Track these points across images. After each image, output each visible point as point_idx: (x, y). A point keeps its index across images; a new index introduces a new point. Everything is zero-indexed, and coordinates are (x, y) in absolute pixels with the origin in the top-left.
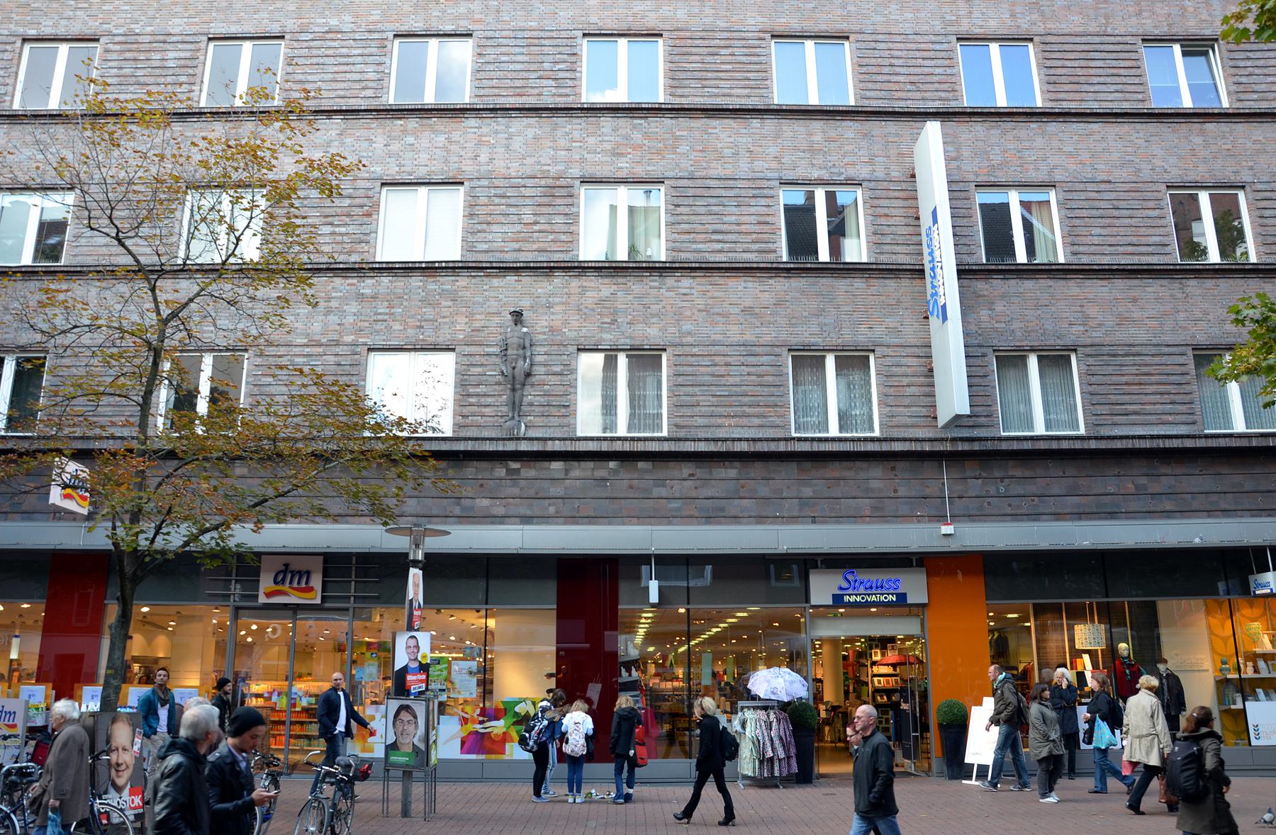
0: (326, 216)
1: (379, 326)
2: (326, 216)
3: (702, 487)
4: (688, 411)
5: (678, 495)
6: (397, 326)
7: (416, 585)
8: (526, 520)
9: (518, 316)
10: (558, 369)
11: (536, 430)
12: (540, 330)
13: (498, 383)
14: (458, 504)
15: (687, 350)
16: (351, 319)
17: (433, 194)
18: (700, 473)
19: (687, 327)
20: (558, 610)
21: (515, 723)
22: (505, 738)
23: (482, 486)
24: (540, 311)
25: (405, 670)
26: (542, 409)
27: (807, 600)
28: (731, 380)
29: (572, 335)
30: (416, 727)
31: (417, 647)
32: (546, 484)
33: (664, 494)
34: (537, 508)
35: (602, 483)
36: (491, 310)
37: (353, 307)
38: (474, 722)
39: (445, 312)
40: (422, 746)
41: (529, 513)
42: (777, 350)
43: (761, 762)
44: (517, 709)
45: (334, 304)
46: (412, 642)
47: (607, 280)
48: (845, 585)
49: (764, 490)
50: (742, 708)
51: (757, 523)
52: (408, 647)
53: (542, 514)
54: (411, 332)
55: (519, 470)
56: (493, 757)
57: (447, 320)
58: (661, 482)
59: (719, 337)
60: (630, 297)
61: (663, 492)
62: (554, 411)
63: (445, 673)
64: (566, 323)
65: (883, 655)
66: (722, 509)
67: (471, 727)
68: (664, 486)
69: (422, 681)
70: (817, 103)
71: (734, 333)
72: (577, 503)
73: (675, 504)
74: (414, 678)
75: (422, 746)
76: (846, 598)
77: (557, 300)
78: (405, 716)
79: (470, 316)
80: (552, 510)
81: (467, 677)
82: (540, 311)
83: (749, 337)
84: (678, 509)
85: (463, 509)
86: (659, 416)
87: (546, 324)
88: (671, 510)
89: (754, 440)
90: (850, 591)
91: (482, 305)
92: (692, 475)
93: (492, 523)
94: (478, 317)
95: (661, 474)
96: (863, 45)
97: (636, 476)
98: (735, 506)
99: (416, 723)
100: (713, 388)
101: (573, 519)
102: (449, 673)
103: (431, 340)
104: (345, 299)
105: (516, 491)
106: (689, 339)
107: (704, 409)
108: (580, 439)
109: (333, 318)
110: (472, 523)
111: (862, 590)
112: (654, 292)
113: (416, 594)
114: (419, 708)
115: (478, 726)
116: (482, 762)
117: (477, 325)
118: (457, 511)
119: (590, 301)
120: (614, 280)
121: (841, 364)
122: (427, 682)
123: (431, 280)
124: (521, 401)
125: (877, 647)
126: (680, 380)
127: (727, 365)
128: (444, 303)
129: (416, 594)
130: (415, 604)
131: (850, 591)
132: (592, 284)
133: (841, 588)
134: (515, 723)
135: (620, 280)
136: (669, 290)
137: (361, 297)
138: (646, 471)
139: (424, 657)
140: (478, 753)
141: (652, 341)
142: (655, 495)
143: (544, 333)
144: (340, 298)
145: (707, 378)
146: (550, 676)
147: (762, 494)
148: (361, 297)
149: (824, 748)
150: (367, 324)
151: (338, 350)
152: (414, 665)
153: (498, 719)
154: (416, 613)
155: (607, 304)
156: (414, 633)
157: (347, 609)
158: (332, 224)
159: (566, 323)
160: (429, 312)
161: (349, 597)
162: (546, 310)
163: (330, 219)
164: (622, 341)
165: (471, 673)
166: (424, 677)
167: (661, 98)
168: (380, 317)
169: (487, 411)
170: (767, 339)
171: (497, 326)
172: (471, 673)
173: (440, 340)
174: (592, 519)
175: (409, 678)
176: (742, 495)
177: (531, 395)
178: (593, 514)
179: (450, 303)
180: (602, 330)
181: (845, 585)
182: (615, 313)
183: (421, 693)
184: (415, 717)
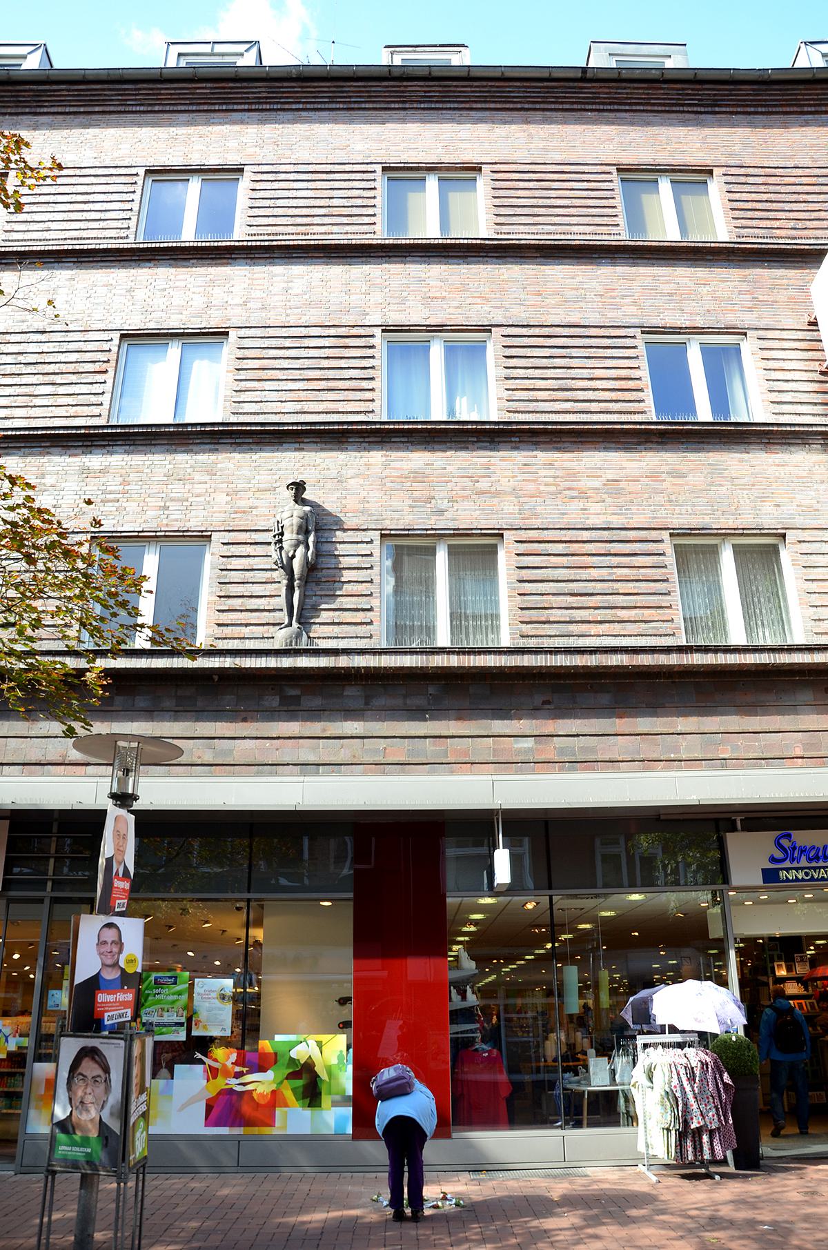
6: (132, 506)
7: (120, 836)
17: (190, 351)
20: (357, 900)
21: (291, 1076)
22: (275, 1099)
25: (94, 984)
27: (726, 880)
30: (108, 1089)
31: (119, 943)
36: (262, 486)
38: (227, 1074)
40: (115, 1126)
43: (682, 1136)
44: (293, 1054)
46: (110, 935)
48: (779, 854)
50: (646, 1046)
52: (101, 943)
55: (298, 698)
56: (255, 1130)
57: (202, 499)
63: (185, 997)
65: (789, 969)
67: (221, 1083)
69: (124, 1004)
70: (309, 1133)
74: (111, 998)
75: (115, 1126)
76: (783, 874)
78: (89, 1068)
81: (217, 1003)
88: (519, 751)
90: (787, 864)
96: (730, 179)
99: (107, 1082)
102: (191, 997)
111: (804, 862)
113: (120, 850)
114: (114, 1052)
115: (234, 1081)
116: (239, 1141)
117: (243, 504)
121: (740, 553)
122: (138, 1006)
125: (780, 959)
129: (120, 850)
130: (118, 868)
131: (787, 864)
133: (773, 859)
134: (291, 1076)
139: (131, 961)
140: (232, 1125)
146: (343, 1001)
149: (203, 1063)
152: (111, 975)
153: (262, 1069)
154: (118, 884)
156: (117, 920)
157: (41, 901)
161: (45, 882)
165: (223, 997)
166: (129, 997)
167: (445, 419)
172: (223, 997)
175: (101, 997)
178: (408, 760)
181: (779, 854)
183: (121, 1026)
184: (106, 1070)
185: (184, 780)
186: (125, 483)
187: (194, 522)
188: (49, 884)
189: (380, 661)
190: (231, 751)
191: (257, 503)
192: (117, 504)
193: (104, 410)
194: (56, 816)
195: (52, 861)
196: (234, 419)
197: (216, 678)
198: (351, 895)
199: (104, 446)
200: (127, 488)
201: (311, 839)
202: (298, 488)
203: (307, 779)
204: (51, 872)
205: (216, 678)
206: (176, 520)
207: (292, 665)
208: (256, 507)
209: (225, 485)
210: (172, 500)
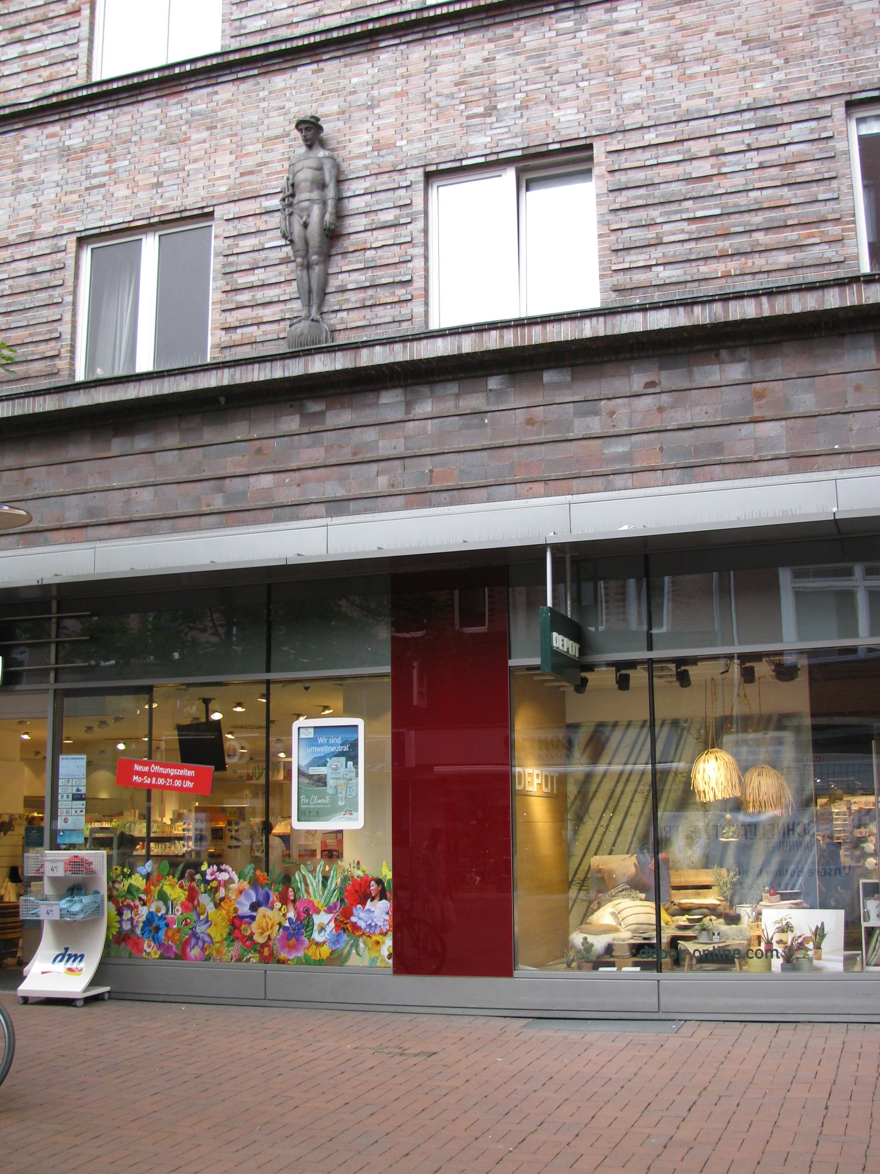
0: (13, 29)
1: (95, 197)
2: (13, 29)
3: (673, 406)
4: (639, 259)
5: (624, 428)
6: (121, 191)
8: (337, 506)
9: (311, 130)
10: (388, 217)
11: (362, 325)
12: (358, 151)
13: (285, 261)
14: (220, 490)
15: (635, 139)
16: (50, 194)
18: (668, 378)
19: (632, 94)
23: (259, 451)
24: (357, 115)
26: (361, 295)
28: (727, 184)
29: (417, 147)
32: (370, 435)
33: (597, 430)
34: (358, 480)
35: (475, 420)
36: (272, 133)
37: (54, 173)
39: (197, 151)
41: (341, 493)
42: (824, 108)
45: (27, 173)
47: (474, 37)
49: (805, 400)
51: (792, 471)
53: (364, 491)
54: (143, 196)
58: (588, 407)
59: (700, 103)
60: (521, 59)
61: (595, 425)
62: (384, 295)
64: (402, 127)
66: (718, 447)
68: (596, 413)
71: (729, 92)
72: (427, 464)
73: (619, 447)
77: (385, 91)
79: (239, 153)
80: (382, 483)
82: (357, 115)
83: (762, 89)
84: (627, 457)
85: (228, 500)
86: (484, 613)
87: (367, 137)
89: (770, 293)
91: (256, 126)
92: (652, 384)
93: (277, 520)
94: (251, 149)
95: (590, 389)
97: (539, 400)
98: (743, 439)
100: (689, 204)
101: (420, 497)
103: (174, 205)
104: (41, 162)
105: (317, 455)
106: (636, 118)
107: (671, 250)
108: (442, 334)
109: (26, 198)
110: (244, 523)
112: (566, 42)
117: (249, 163)
118: (218, 503)
119: (447, 79)
120: (490, 34)
123: (173, 100)
124: (324, 284)
126: (622, 199)
127: (718, 154)
128: (195, 137)
132: (448, 49)
135: (501, 31)
136: (594, 29)
137: (66, 154)
138: (558, 386)
141: (566, 134)
142: (576, 433)
143: (364, 156)
144: (35, 161)
145: (675, 186)
147: (801, 410)
148: (66, 154)
150: (75, 197)
151: (34, 249)
155: (477, 81)
158: (21, 41)
159: (402, 127)
160: (171, 156)
161: (46, 672)
162: (367, 113)
163: (17, 34)
164: (507, 143)
168: (95, 182)
169: (268, 313)
170: (799, 90)
171: (281, 157)
173: (189, 203)
174: (457, 492)
176: (757, 414)
177: (346, 273)
179: (205, 134)
180: (467, 129)
182: (493, 93)
185: (66, 547)
186: (111, 160)
187: (193, 198)
188: (52, 675)
189: (544, 334)
190: (244, 493)
191: (267, 157)
192: (103, 190)
193: (83, 71)
194: (54, 592)
195: (53, 647)
196: (235, 44)
197: (222, 400)
198: (387, 669)
199: (84, 115)
200: (114, 166)
201: (605, 583)
202: (311, 130)
203: (336, 520)
204: (53, 660)
205: (222, 400)
206: (173, 199)
207: (349, 365)
208: (265, 163)
209: (228, 140)
210: (166, 172)
